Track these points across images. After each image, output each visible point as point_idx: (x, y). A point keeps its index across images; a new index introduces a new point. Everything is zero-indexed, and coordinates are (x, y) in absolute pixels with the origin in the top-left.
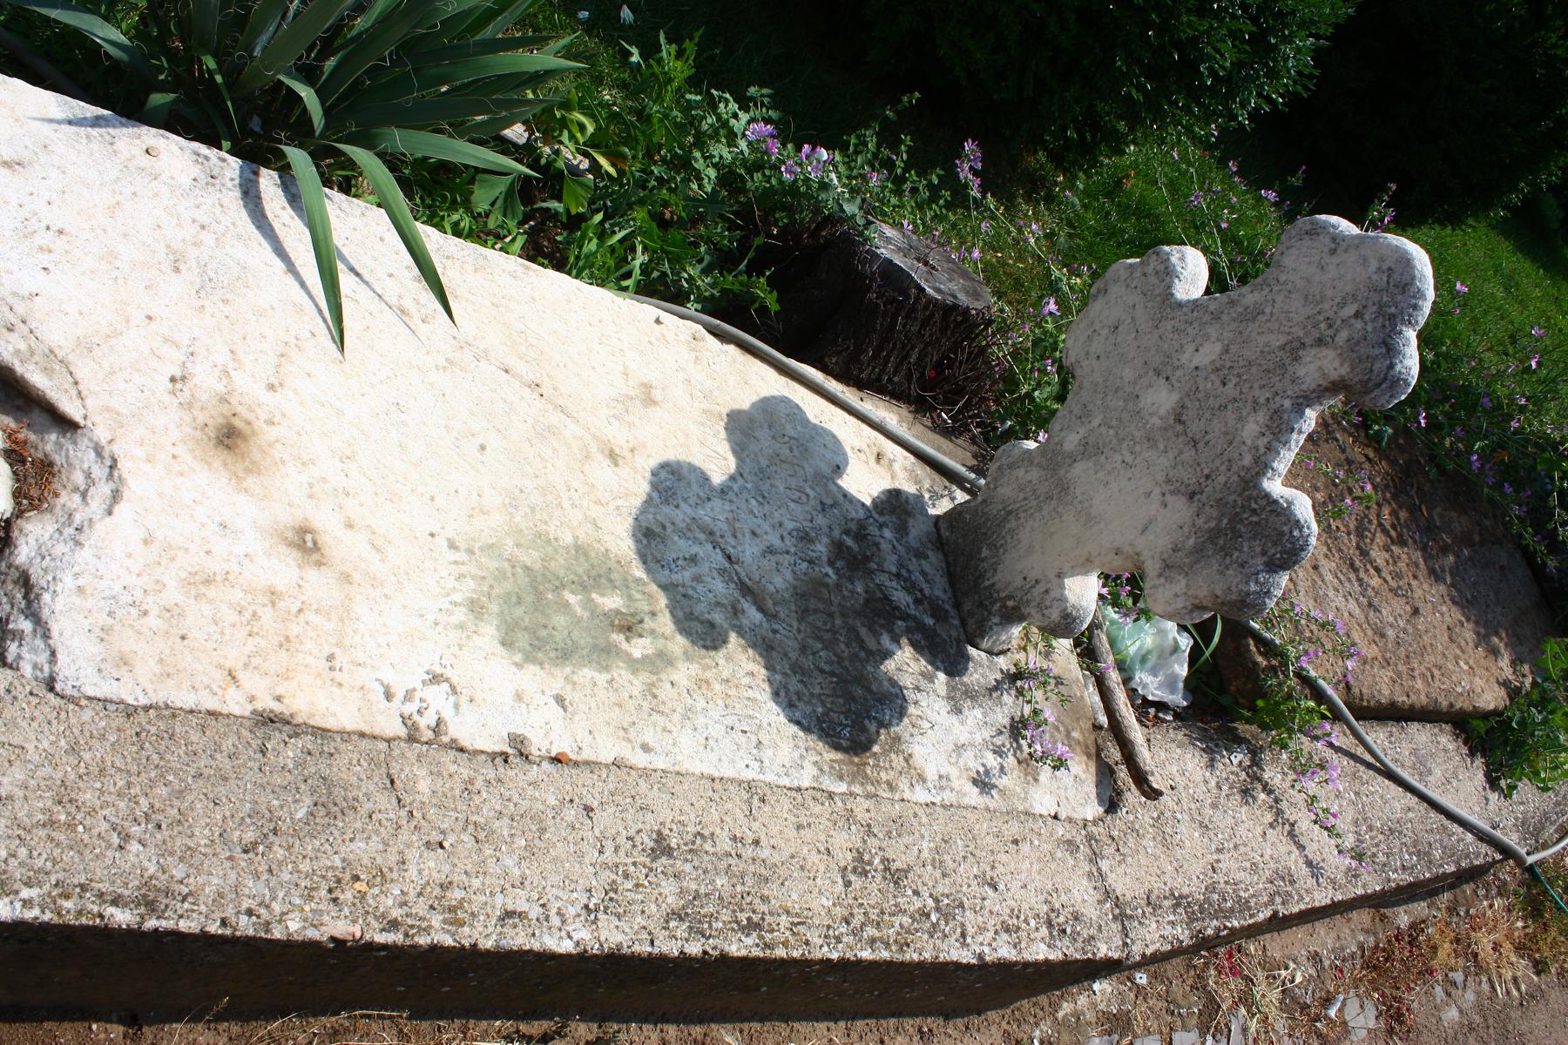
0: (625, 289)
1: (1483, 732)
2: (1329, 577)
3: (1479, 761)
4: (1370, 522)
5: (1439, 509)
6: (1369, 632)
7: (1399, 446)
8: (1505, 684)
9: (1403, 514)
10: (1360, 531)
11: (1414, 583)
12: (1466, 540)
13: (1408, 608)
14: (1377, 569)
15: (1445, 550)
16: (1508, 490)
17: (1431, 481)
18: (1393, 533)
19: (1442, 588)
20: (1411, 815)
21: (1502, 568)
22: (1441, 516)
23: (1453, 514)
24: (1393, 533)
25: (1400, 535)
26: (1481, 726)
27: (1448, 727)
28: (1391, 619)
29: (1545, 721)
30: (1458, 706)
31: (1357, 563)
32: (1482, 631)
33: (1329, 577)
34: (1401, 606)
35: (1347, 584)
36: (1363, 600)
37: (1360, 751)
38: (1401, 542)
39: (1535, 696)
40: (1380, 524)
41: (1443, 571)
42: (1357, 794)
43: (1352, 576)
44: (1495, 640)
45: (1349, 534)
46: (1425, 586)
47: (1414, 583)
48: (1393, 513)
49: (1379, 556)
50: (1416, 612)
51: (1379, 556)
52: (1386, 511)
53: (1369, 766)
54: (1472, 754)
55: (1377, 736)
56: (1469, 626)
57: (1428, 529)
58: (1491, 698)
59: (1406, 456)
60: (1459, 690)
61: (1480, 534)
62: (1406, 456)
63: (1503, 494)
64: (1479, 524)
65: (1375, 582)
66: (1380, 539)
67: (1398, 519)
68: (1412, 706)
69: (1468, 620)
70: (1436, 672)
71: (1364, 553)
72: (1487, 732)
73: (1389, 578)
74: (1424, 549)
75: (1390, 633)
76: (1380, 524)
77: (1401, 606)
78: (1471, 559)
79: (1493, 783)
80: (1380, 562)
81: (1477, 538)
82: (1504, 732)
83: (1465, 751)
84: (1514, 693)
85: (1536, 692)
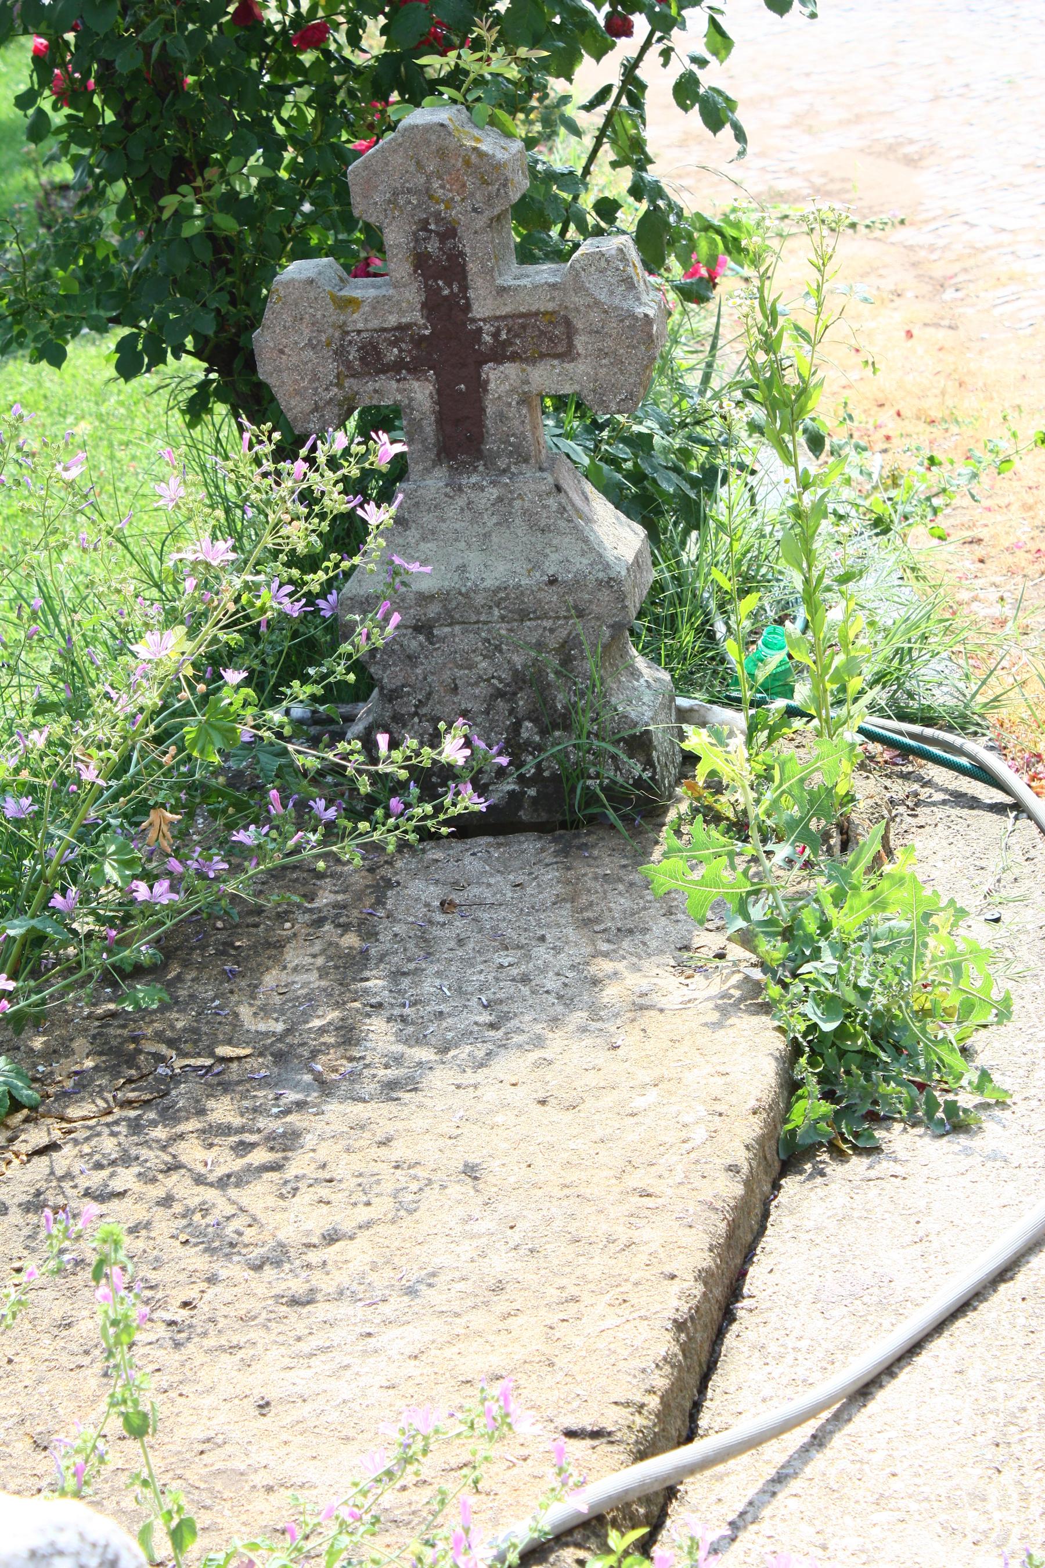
0: (640, 1501)
1: (826, 1107)
2: (302, 1379)
3: (896, 1138)
4: (205, 1210)
5: (245, 1012)
6: (478, 1319)
7: (51, 1054)
8: (726, 1008)
9: (223, 1110)
10: (220, 1246)
11: (399, 1151)
12: (348, 968)
13: (455, 1190)
14: (331, 1238)
15: (348, 1035)
16: (247, 836)
17: (164, 1008)
18: (260, 1156)
19: (440, 1079)
20: (974, 1374)
21: (446, 906)
22: (264, 1011)
23: (270, 979)
24: (260, 1156)
25: (272, 1141)
26: (810, 1109)
27: (790, 1184)
28: (467, 1250)
29: (842, 949)
30: (742, 1157)
31: (297, 1286)
32: (579, 1017)
33: (302, 1379)
34: (446, 1208)
35: (337, 1335)
36: (398, 1303)
37: (776, 1453)
38: (287, 1142)
39: (775, 950)
40: (223, 1183)
41: (398, 1060)
42: (880, 1501)
43: (320, 1311)
44: (611, 993)
45: (212, 1280)
46: (419, 1122)
47: (399, 1151)
48: (211, 1134)
49: (296, 1220)
50: (471, 1172)
51: (296, 1220)
52: (192, 1152)
53: (818, 1441)
54: (873, 1150)
55: (746, 1392)
56: (556, 1041)
57: (280, 1058)
58: (750, 1059)
59: (80, 1044)
60: (699, 1134)
61: (345, 928)
62: (80, 1044)
63: (258, 852)
64: (319, 922)
65: (356, 1254)
66: (257, 1195)
67: (226, 1130)
68: (705, 1277)
69: (539, 1042)
70: (636, 1180)
71: (279, 1257)
72: (828, 1096)
73: (363, 1214)
74: (325, 1087)
75: (500, 1264)
76: (223, 1183)
77: (446, 1208)
78: (397, 975)
79: (956, 1124)
80: (317, 1222)
81: (351, 940)
82: (842, 1054)
83: (858, 1164)
84: (754, 999)
85: (764, 945)
